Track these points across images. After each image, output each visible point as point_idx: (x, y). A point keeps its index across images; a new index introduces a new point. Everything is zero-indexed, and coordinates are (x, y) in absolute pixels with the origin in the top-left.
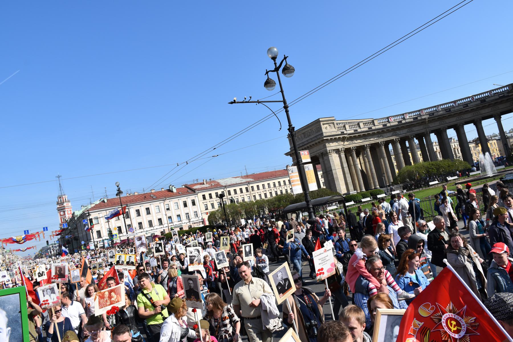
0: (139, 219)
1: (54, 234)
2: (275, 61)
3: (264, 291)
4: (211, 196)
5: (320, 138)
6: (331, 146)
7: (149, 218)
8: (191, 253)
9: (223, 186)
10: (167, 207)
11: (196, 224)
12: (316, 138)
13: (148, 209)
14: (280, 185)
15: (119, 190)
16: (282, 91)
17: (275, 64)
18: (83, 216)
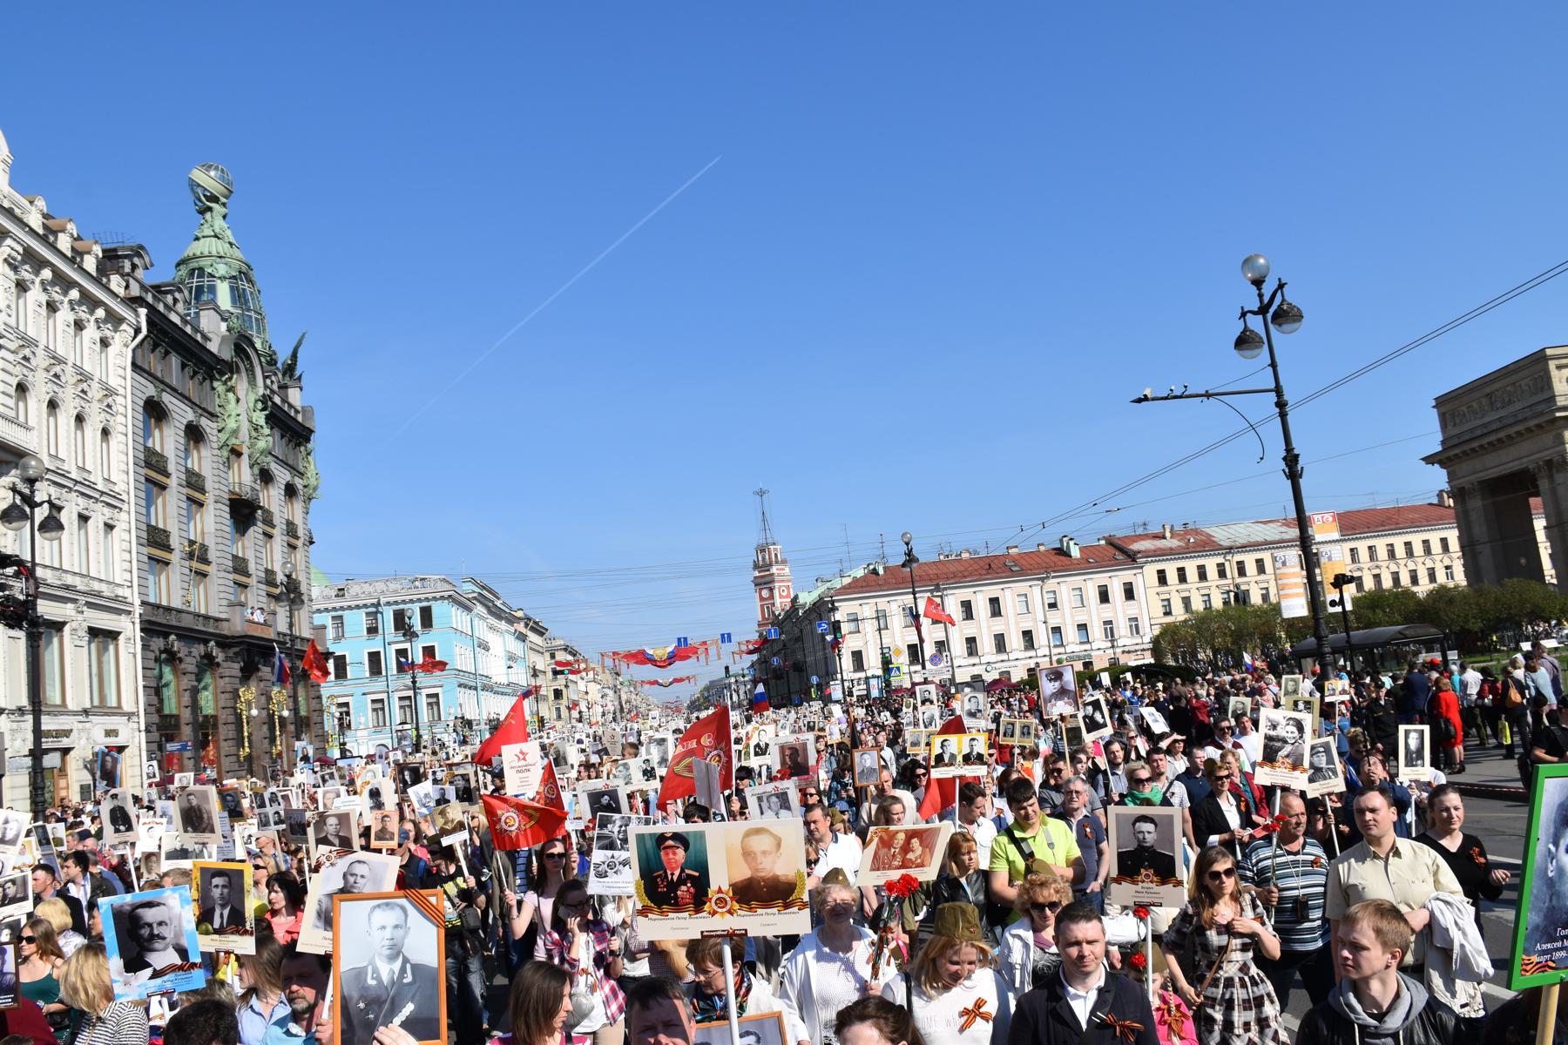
1: (744, 648)
2: (1259, 289)
3: (1436, 882)
4: (1202, 575)
5: (1541, 414)
7: (998, 626)
8: (1274, 727)
10: (1049, 599)
11: (1132, 656)
13: (994, 602)
14: (1410, 552)
15: (909, 553)
16: (1273, 365)
17: (1261, 296)
18: (823, 608)
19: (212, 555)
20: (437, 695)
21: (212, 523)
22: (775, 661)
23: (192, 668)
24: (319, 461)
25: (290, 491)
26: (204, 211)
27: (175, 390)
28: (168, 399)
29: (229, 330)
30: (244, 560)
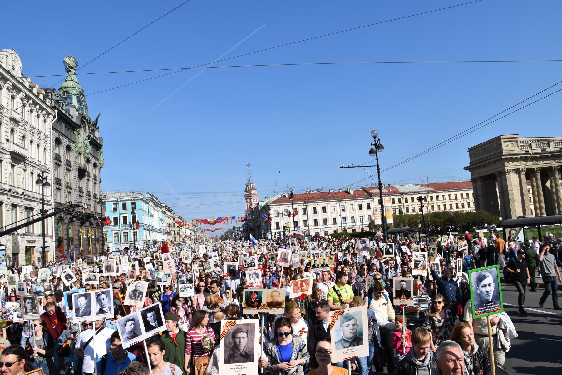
0: (315, 217)
5: (498, 156)
6: (509, 166)
7: (325, 216)
9: (400, 193)
10: (342, 208)
12: (495, 156)
14: (462, 197)
16: (377, 159)
18: (266, 208)
19: (73, 187)
20: (127, 233)
21: (73, 175)
22: (250, 225)
23: (67, 222)
24: (105, 155)
25: (95, 165)
26: (68, 71)
27: (63, 135)
28: (62, 138)
29: (79, 114)
30: (60, 180)
